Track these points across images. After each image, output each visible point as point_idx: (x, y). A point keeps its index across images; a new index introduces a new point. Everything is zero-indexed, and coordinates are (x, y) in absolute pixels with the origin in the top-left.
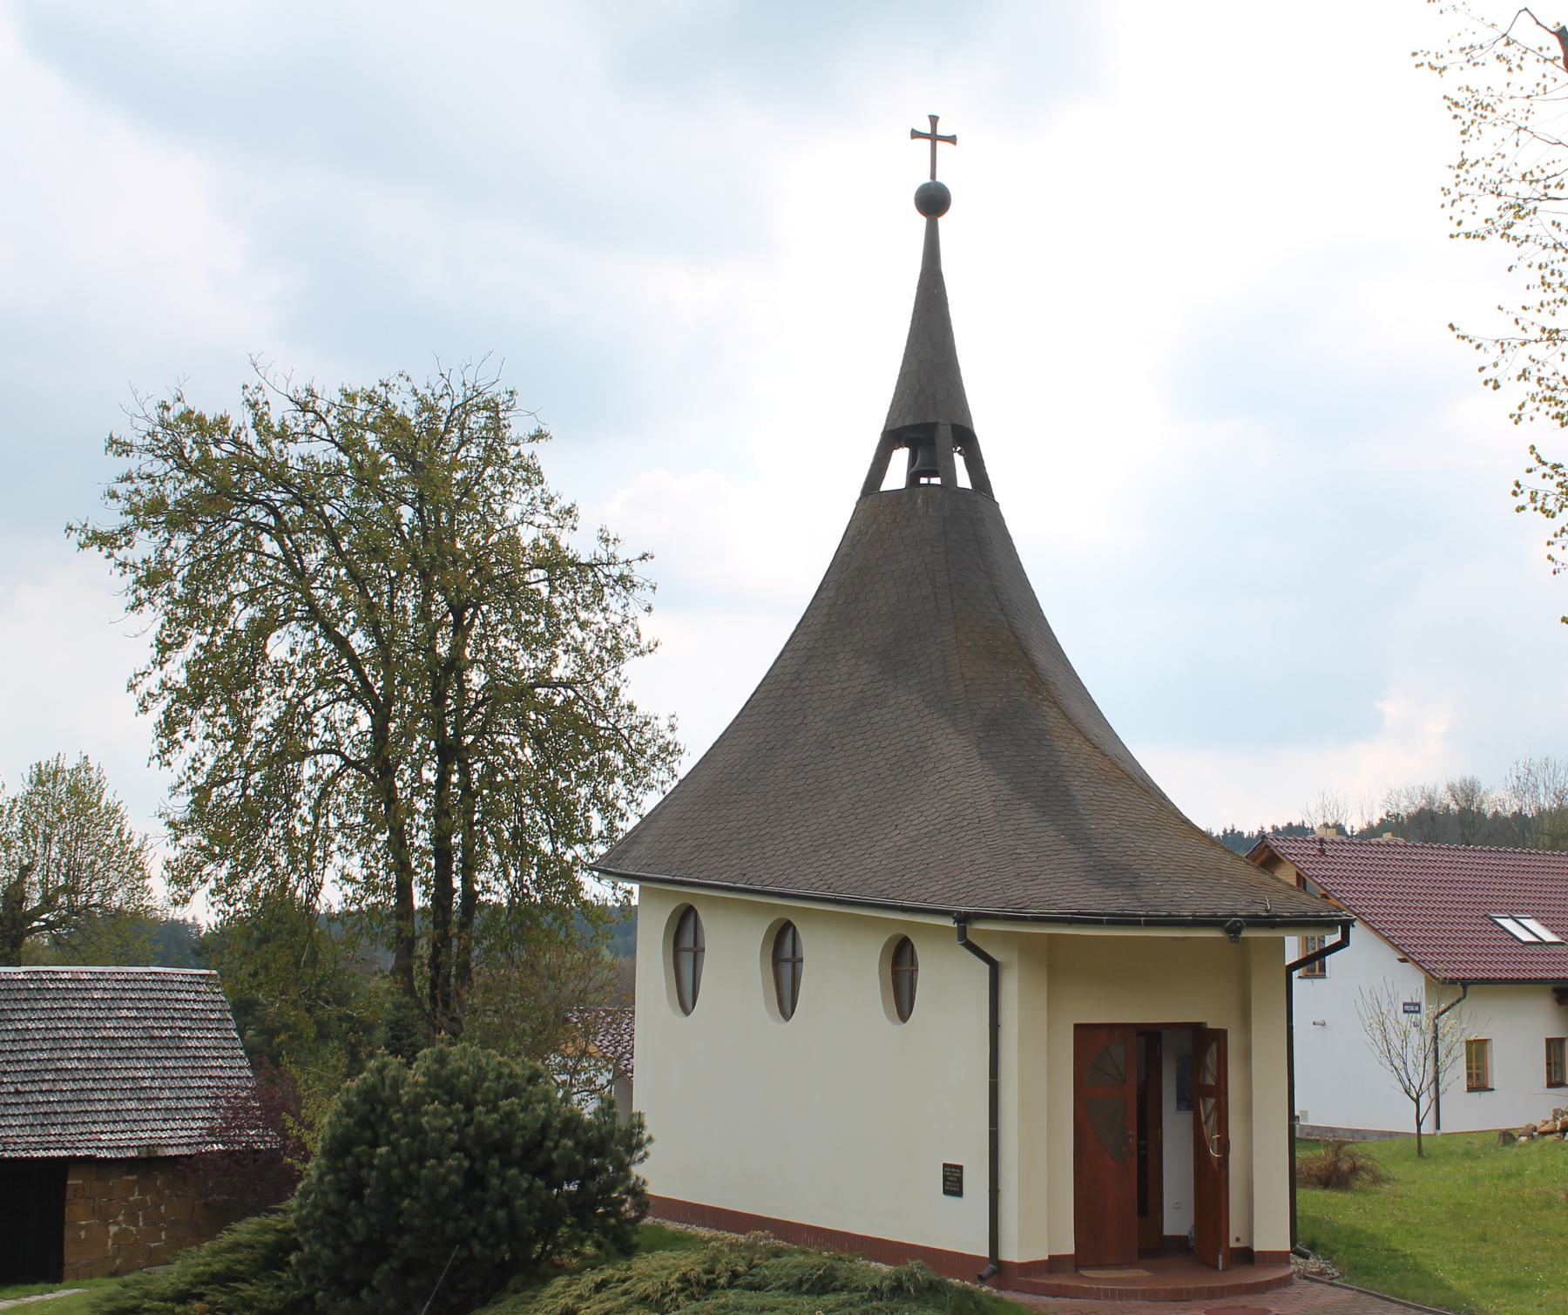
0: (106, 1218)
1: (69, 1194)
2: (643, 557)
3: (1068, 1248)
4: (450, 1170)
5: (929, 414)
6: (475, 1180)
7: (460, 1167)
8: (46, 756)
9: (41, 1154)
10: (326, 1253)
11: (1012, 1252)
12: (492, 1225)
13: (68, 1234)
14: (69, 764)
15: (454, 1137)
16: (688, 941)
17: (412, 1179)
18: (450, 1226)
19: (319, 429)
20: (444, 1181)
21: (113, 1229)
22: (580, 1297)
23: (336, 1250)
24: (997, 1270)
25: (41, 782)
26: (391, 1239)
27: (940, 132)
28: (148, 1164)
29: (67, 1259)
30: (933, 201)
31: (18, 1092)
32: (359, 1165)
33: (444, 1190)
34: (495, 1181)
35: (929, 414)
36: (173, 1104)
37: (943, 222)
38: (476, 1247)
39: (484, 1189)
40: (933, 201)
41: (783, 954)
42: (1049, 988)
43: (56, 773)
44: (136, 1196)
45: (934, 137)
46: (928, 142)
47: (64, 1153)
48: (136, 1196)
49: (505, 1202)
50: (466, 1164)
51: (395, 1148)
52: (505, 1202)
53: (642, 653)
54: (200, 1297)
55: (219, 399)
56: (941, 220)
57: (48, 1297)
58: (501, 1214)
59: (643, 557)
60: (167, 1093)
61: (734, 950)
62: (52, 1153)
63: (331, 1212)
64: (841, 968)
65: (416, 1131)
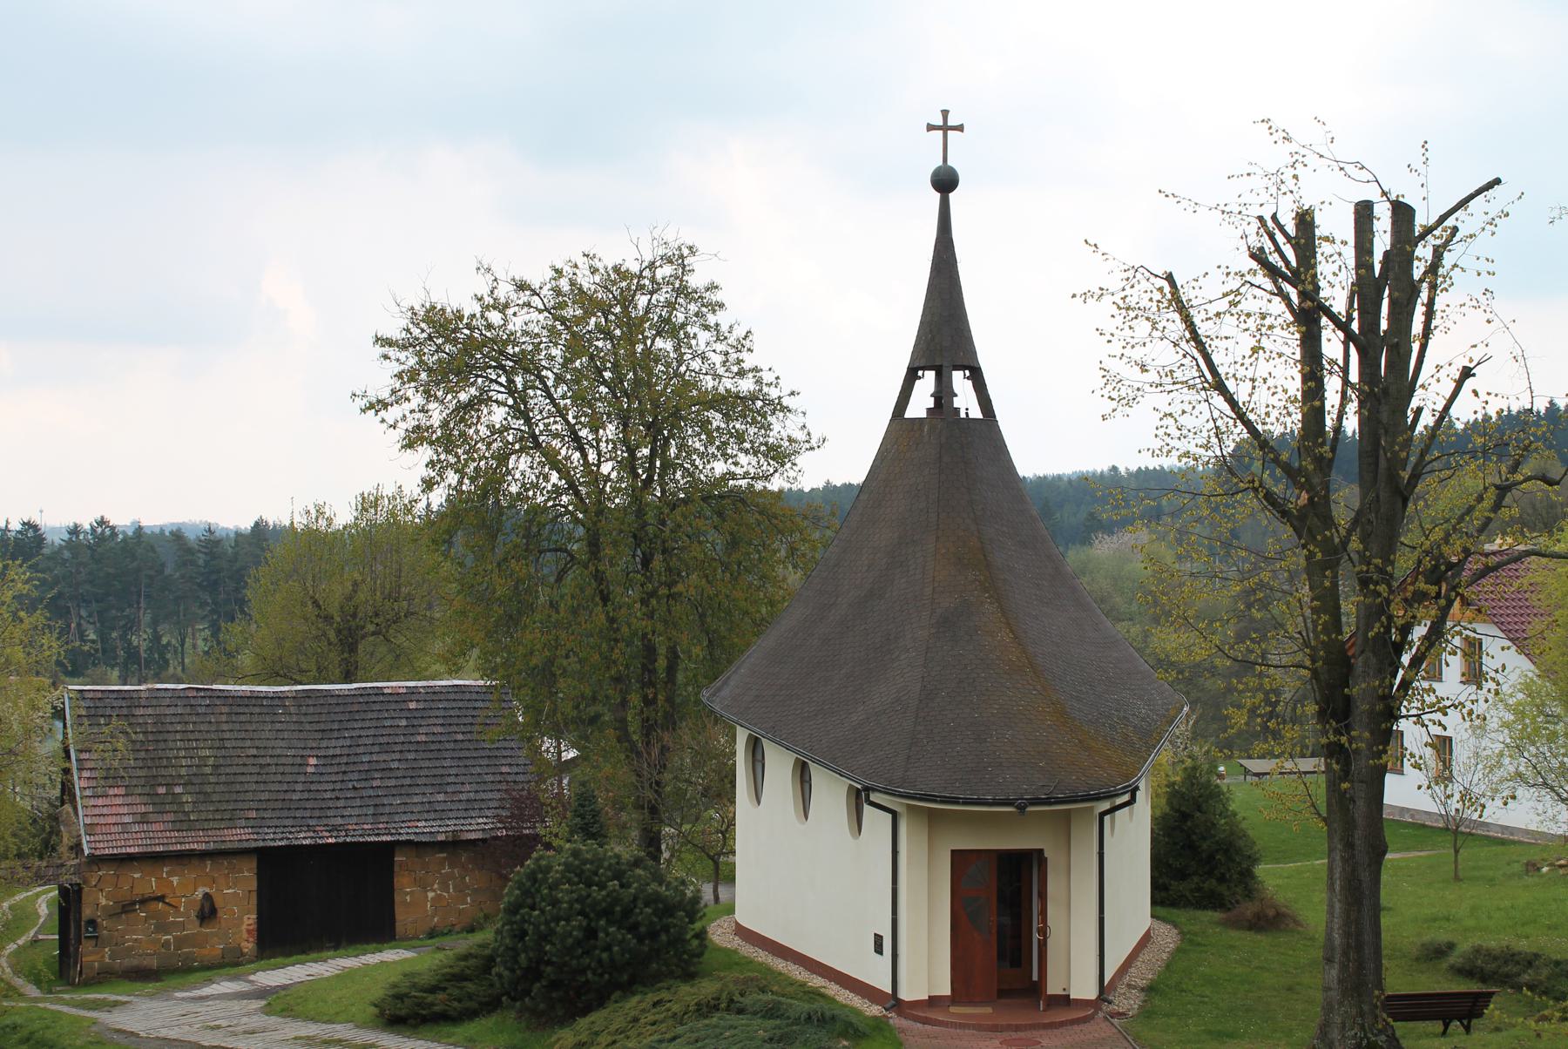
0: (425, 888)
1: (396, 868)
2: (792, 393)
3: (946, 990)
4: (574, 928)
5: (945, 339)
6: (591, 933)
7: (580, 926)
8: (368, 488)
9: (372, 839)
10: (506, 973)
11: (905, 994)
12: (600, 961)
13: (397, 898)
14: (388, 490)
15: (577, 906)
16: (759, 757)
17: (552, 932)
18: (574, 962)
19: (536, 301)
20: (570, 934)
21: (431, 895)
22: (643, 1011)
23: (512, 971)
24: (893, 1001)
25: (364, 509)
26: (542, 967)
27: (940, 133)
28: (454, 845)
29: (398, 917)
30: (945, 182)
31: (354, 788)
32: (524, 921)
33: (570, 941)
34: (601, 935)
35: (945, 339)
36: (472, 795)
37: (953, 196)
38: (590, 975)
39: (596, 938)
40: (945, 182)
41: (802, 775)
42: (930, 827)
43: (377, 499)
44: (447, 870)
45: (945, 128)
46: (940, 133)
47: (389, 838)
48: (447, 870)
49: (608, 948)
50: (584, 923)
51: (543, 911)
52: (608, 948)
53: (812, 449)
54: (444, 989)
55: (460, 295)
56: (952, 196)
57: (372, 959)
58: (605, 956)
59: (792, 393)
60: (467, 787)
61: (779, 766)
62: (385, 838)
63: (508, 948)
64: (830, 792)
65: (555, 903)
